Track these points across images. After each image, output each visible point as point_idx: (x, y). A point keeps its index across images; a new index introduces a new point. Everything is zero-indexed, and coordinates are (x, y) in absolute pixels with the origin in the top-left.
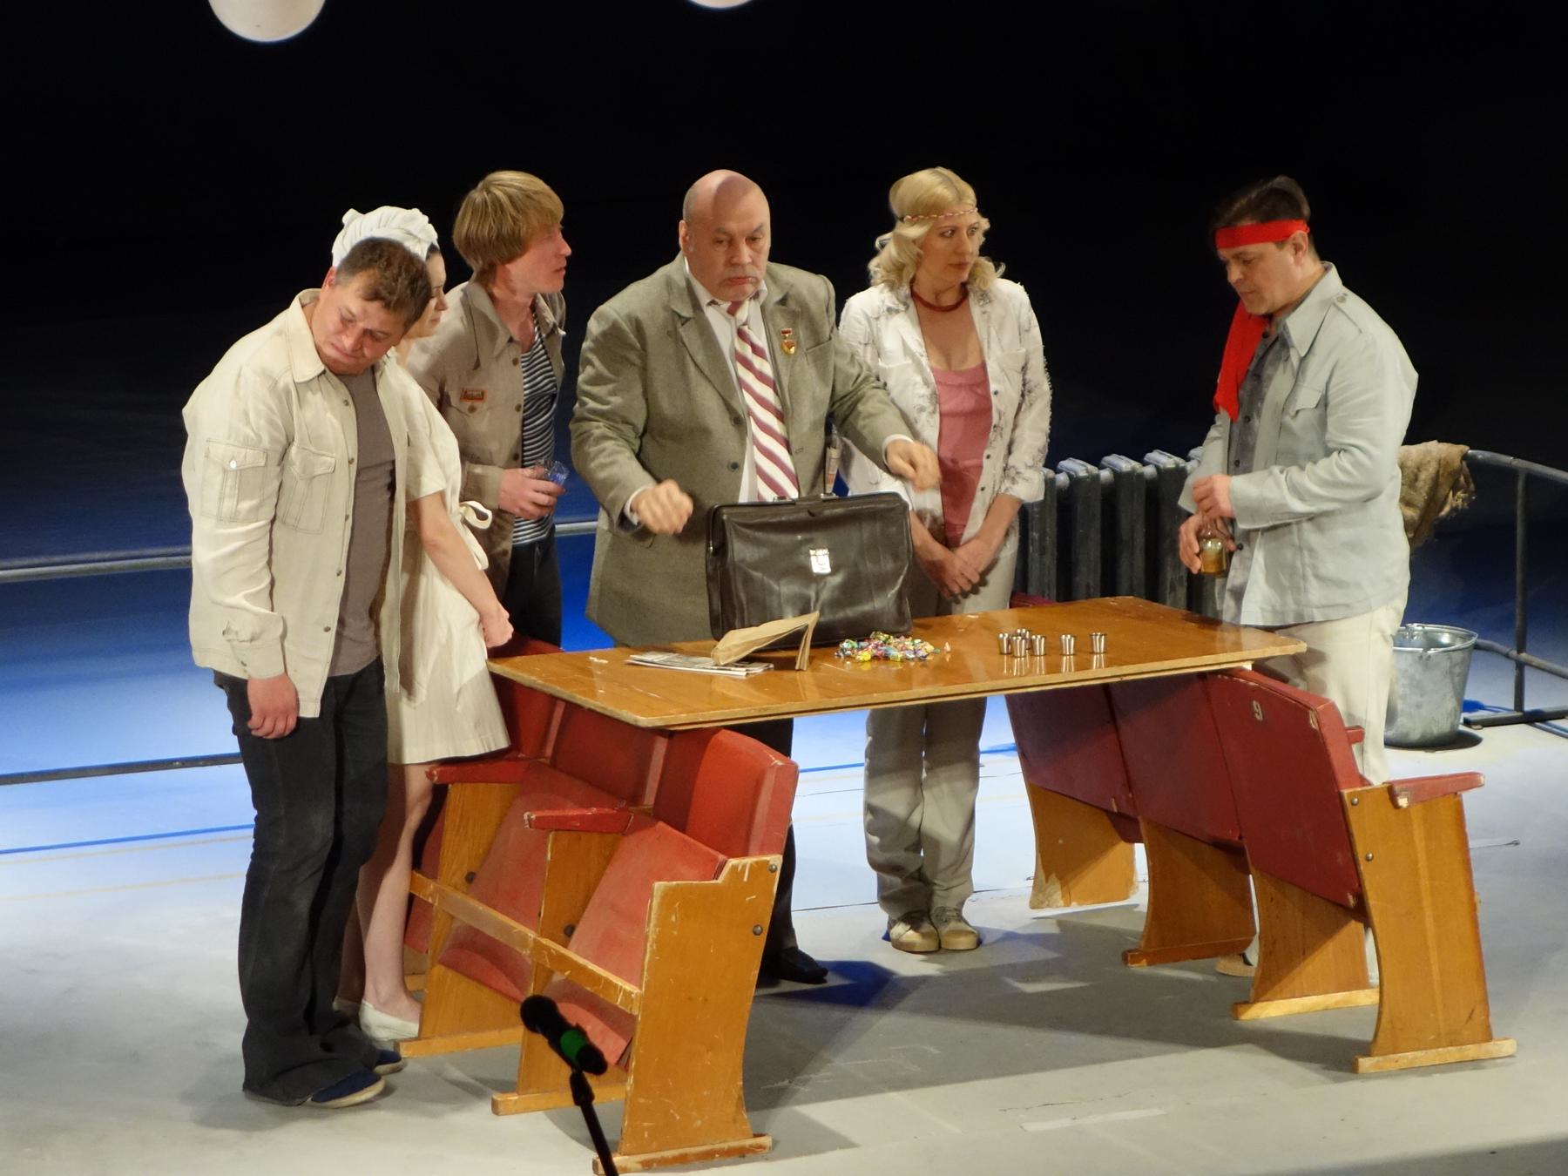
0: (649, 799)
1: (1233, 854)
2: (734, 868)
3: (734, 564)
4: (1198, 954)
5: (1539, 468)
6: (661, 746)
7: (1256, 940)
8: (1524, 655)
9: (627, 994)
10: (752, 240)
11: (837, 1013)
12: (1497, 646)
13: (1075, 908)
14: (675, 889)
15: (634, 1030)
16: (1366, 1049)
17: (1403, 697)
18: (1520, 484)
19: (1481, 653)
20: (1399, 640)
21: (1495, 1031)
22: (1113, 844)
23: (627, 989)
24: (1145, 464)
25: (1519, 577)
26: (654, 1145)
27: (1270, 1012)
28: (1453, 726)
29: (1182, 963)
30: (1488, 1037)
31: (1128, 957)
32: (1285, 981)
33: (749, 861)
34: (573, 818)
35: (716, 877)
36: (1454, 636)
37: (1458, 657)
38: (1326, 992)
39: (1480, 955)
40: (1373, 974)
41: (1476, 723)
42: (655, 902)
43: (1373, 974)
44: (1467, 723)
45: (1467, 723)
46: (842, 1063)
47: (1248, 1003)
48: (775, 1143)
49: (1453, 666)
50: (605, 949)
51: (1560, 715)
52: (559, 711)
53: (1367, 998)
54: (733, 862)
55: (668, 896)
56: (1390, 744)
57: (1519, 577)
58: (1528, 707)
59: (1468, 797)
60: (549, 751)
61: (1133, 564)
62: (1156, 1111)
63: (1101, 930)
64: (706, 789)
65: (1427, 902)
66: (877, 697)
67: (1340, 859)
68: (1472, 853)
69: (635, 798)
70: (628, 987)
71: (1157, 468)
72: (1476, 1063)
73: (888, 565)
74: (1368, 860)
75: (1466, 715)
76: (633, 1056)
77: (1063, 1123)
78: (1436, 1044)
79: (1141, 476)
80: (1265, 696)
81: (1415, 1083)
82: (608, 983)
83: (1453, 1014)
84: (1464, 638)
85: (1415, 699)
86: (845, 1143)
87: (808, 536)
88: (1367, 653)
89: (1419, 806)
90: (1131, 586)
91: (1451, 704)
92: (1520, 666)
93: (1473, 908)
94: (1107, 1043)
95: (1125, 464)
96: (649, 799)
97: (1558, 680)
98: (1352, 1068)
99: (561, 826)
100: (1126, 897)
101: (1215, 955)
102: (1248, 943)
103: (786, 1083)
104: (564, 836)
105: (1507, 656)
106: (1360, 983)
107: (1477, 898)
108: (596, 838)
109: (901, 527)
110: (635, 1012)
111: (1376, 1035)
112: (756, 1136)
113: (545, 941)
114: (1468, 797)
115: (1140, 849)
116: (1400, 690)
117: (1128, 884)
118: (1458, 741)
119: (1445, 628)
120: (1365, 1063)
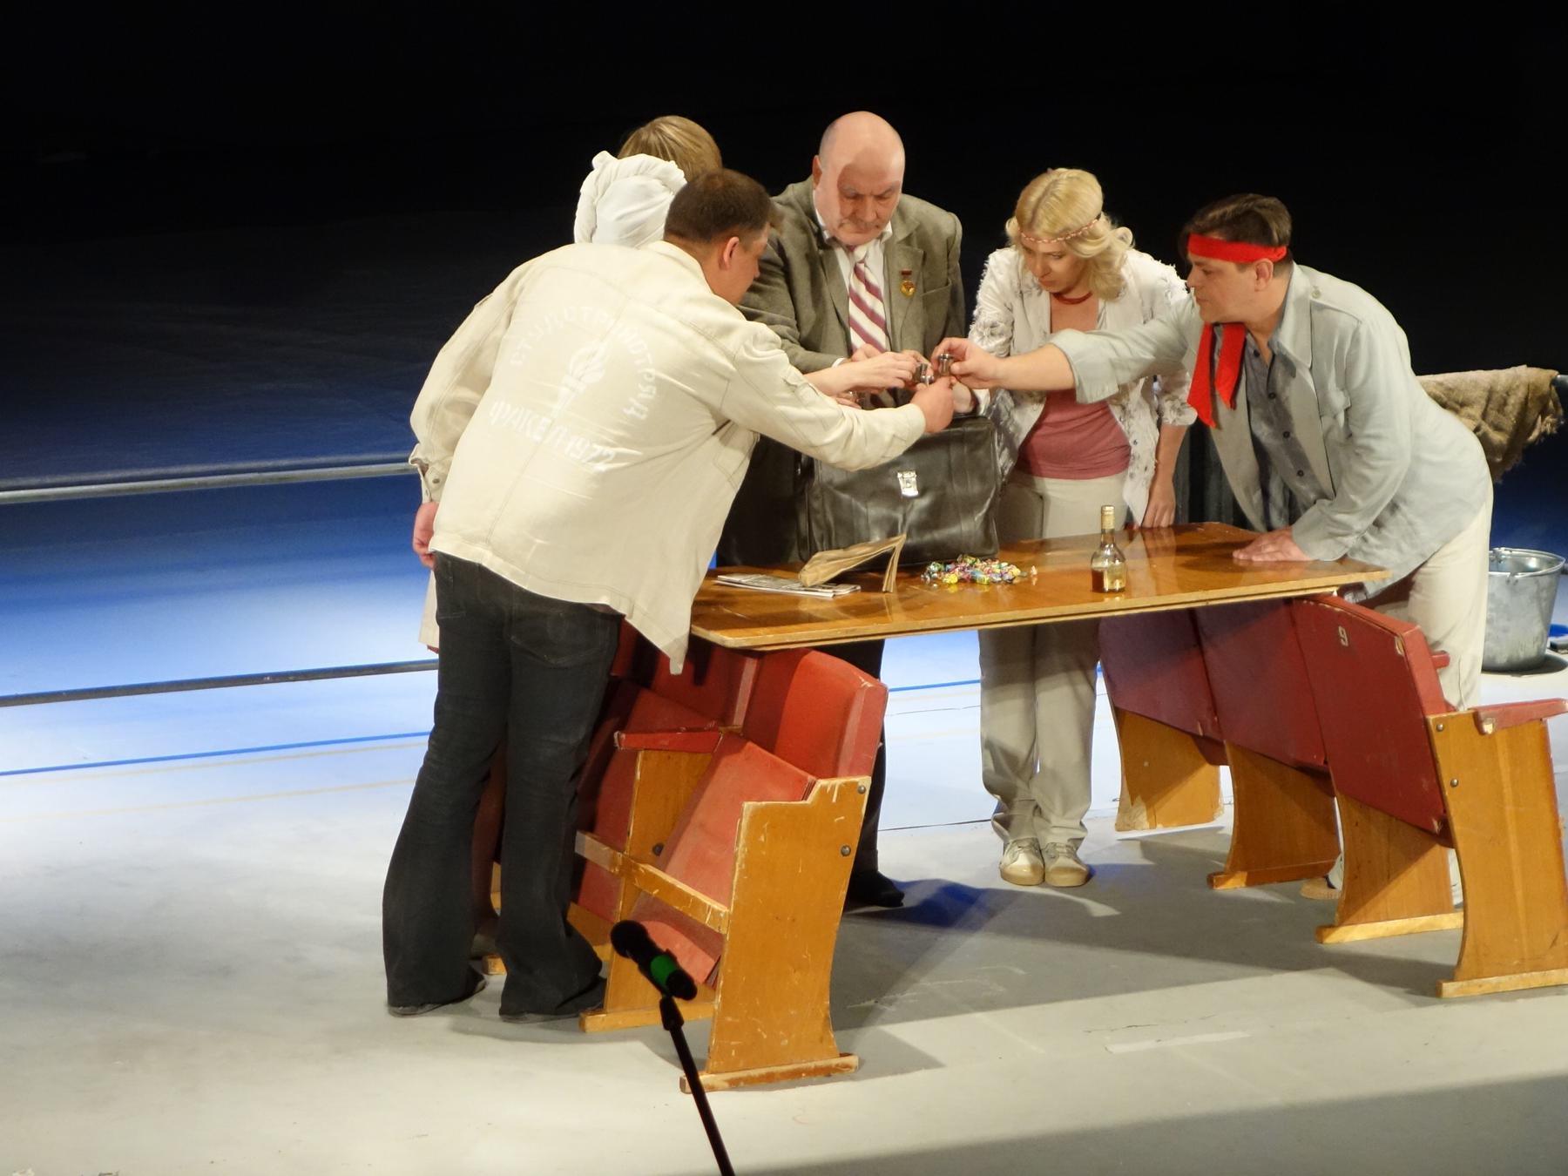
0: (738, 720)
1: (1319, 777)
2: (823, 789)
9: (716, 913)
11: (923, 934)
13: (1160, 830)
14: (763, 810)
15: (721, 949)
16: (1450, 974)
20: (1495, 563)
22: (1195, 768)
23: (715, 909)
26: (741, 1065)
27: (1353, 936)
32: (1368, 906)
35: (805, 797)
36: (1542, 561)
37: (1545, 581)
38: (1410, 916)
42: (745, 822)
44: (1554, 647)
45: (1554, 647)
46: (927, 984)
47: (1332, 927)
48: (861, 1062)
49: (1540, 590)
54: (822, 783)
55: (757, 816)
59: (1553, 723)
62: (1240, 1034)
66: (982, 618)
67: (1425, 784)
68: (1557, 778)
69: (725, 717)
73: (975, 488)
74: (1453, 785)
76: (721, 975)
77: (1148, 1045)
78: (1520, 969)
80: (1347, 619)
81: (1499, 1007)
82: (697, 902)
86: (929, 1063)
89: (1505, 733)
91: (1538, 628)
93: (1558, 833)
96: (738, 720)
98: (1436, 993)
100: (1211, 819)
102: (1330, 866)
104: (654, 755)
106: (1443, 907)
107: (1561, 824)
108: (684, 759)
110: (724, 931)
112: (842, 1055)
114: (1553, 723)
115: (1225, 772)
119: (1533, 553)
120: (1449, 988)
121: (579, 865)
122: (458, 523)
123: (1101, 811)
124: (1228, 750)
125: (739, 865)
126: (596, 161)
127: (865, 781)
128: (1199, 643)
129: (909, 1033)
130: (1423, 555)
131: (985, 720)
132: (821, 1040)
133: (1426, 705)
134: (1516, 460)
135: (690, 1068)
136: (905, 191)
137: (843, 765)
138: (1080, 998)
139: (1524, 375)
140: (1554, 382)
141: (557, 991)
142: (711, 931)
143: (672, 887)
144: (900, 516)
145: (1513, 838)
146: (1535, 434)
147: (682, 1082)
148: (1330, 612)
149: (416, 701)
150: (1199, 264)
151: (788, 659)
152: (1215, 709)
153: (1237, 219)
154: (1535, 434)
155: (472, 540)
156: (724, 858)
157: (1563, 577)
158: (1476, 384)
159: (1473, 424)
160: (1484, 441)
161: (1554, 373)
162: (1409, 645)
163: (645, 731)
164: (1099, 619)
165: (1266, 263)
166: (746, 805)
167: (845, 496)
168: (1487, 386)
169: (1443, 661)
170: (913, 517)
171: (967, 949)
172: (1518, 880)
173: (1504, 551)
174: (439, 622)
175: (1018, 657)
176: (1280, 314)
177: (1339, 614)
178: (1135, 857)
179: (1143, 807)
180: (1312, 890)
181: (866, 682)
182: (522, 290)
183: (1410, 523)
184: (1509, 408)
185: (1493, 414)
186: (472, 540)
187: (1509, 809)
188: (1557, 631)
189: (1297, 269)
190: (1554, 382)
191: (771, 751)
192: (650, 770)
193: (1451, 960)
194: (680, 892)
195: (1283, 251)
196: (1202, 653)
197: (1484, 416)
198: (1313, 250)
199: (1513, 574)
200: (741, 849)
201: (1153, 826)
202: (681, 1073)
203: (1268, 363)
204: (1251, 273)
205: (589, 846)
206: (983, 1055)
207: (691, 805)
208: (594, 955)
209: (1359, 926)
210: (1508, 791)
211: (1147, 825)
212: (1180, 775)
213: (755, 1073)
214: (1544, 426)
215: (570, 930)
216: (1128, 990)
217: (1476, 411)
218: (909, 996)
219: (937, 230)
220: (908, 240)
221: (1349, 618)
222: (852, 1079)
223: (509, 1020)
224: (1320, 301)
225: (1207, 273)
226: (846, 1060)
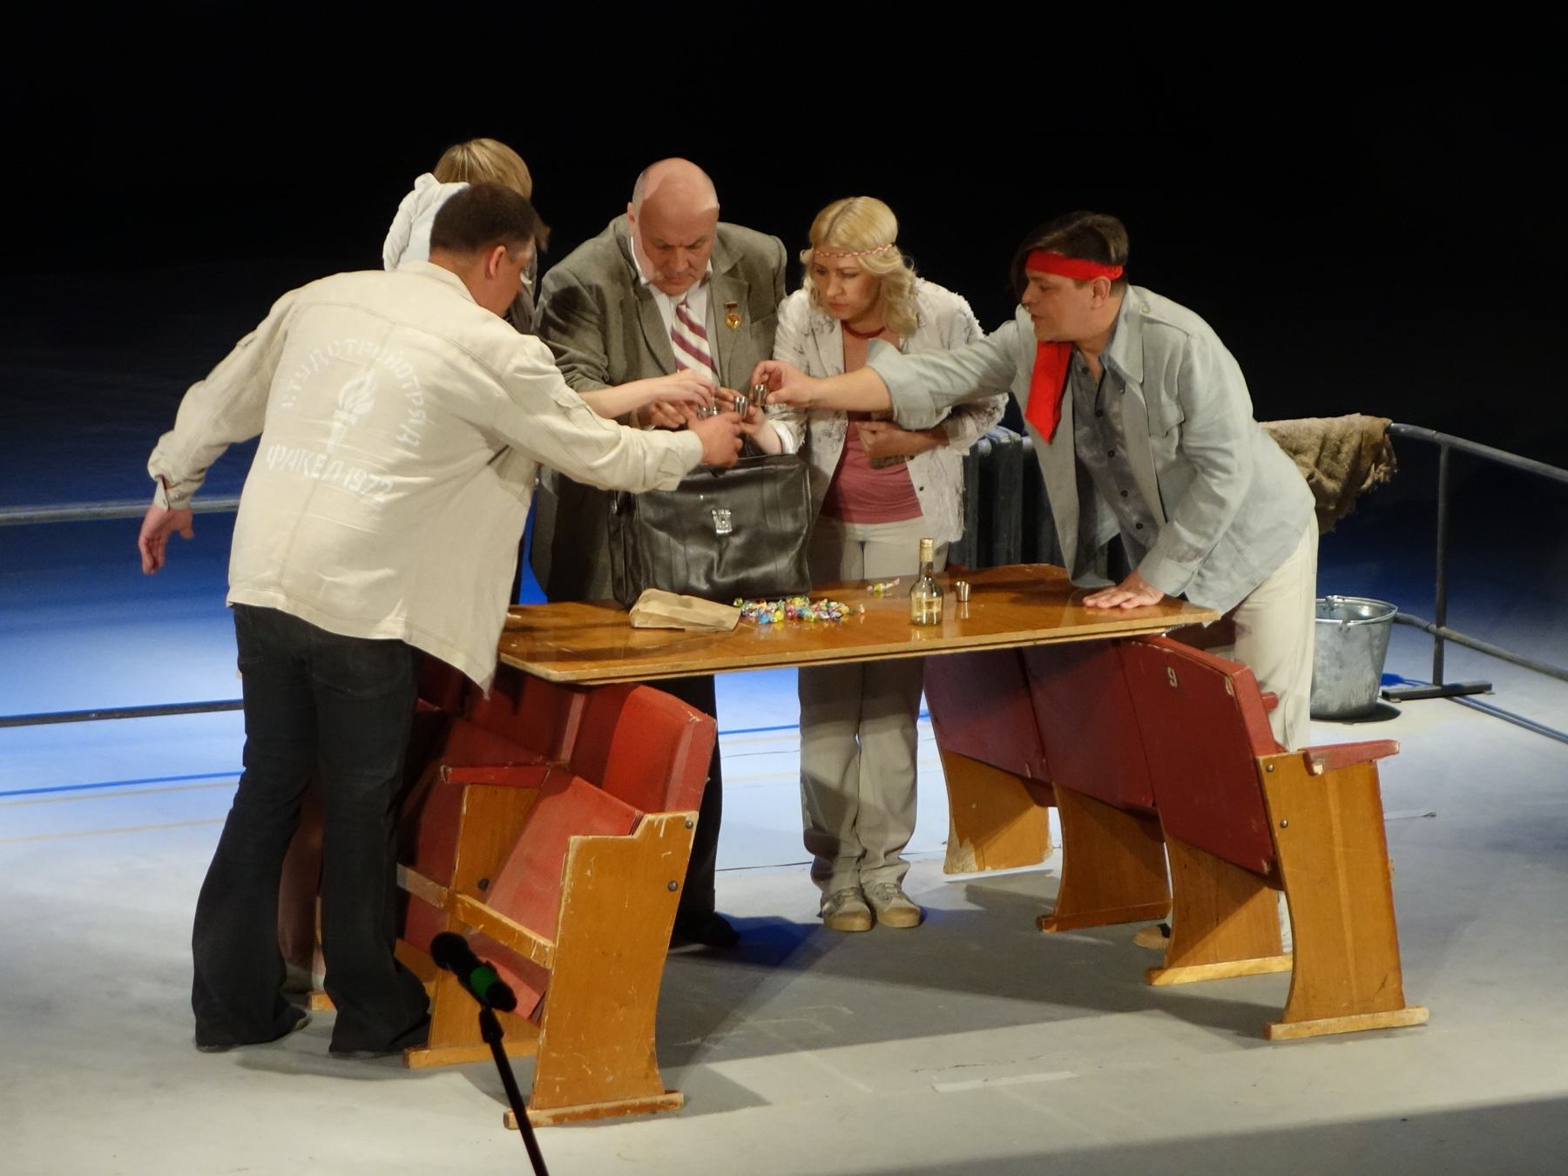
0: (566, 755)
1: (1147, 820)
2: (651, 823)
8: (1443, 629)
9: (541, 948)
12: (1417, 619)
13: (989, 872)
14: (589, 843)
15: (547, 983)
16: (1279, 1016)
20: (1325, 611)
22: (1026, 808)
23: (541, 943)
25: (1439, 551)
27: (1182, 978)
29: (1096, 929)
31: (1042, 922)
33: (665, 816)
35: (632, 832)
37: (1378, 629)
41: (1395, 696)
42: (571, 856)
43: (1288, 949)
44: (1386, 696)
45: (1386, 696)
47: (1161, 969)
48: (687, 1100)
49: (1372, 638)
50: (521, 904)
53: (1280, 965)
54: (649, 817)
55: (584, 849)
58: (1447, 681)
59: (1381, 764)
62: (1067, 1074)
68: (1387, 825)
69: (552, 752)
70: (542, 941)
72: (1387, 1031)
74: (1282, 826)
75: (1385, 688)
77: (973, 1084)
78: (1350, 1011)
81: (1326, 1050)
82: (522, 938)
85: (1335, 671)
86: (755, 1100)
91: (1370, 676)
92: (1440, 640)
93: (1387, 875)
96: (566, 755)
98: (1265, 1035)
100: (1040, 860)
103: (698, 1040)
105: (1427, 630)
106: (1273, 949)
107: (1390, 866)
108: (512, 792)
110: (549, 966)
112: (668, 1092)
114: (1381, 764)
115: (1053, 813)
117: (1039, 850)
119: (1366, 601)
120: (1278, 1030)
121: (403, 899)
122: (269, 562)
123: (927, 852)
125: (565, 900)
127: (693, 816)
128: (1027, 684)
129: (735, 1071)
130: (1253, 583)
131: (805, 756)
133: (1256, 745)
134: (1349, 508)
135: (517, 1102)
136: (720, 220)
137: (669, 803)
139: (1356, 423)
140: (1388, 430)
141: (384, 1030)
143: (498, 921)
144: (714, 554)
146: (1369, 482)
147: (506, 1118)
148: (1160, 652)
149: (224, 741)
150: (1036, 279)
151: (615, 694)
152: (1043, 751)
153: (1071, 239)
154: (1369, 482)
155: (265, 585)
156: (556, 890)
157: (1395, 626)
158: (1309, 431)
159: (1307, 472)
160: (1316, 488)
161: (1387, 421)
162: (1239, 688)
163: (473, 766)
164: (922, 659)
165: (1104, 281)
166: (573, 839)
167: (662, 535)
168: (1321, 433)
169: (1272, 703)
170: (729, 555)
171: (795, 991)
172: (1347, 923)
173: (1337, 599)
174: (242, 667)
175: (842, 696)
176: (1112, 331)
177: (1169, 655)
178: (960, 903)
179: (971, 847)
181: (695, 717)
182: (286, 335)
183: (1239, 551)
184: (1342, 456)
185: (1326, 461)
186: (265, 585)
187: (1339, 850)
189: (1130, 289)
190: (1388, 430)
191: (599, 786)
192: (474, 804)
194: (506, 927)
195: (1120, 271)
196: (1031, 696)
197: (1318, 463)
198: (1141, 273)
199: (1345, 622)
200: (567, 883)
201: (982, 869)
202: (504, 1109)
203: (1097, 380)
204: (1088, 291)
205: (410, 879)
207: (515, 840)
208: (423, 989)
210: (1338, 837)
211: (975, 866)
212: (1006, 817)
214: (1377, 474)
215: (398, 964)
216: (956, 1030)
217: (1310, 459)
218: (735, 1034)
219: (762, 259)
220: (732, 272)
222: (678, 1116)
223: (339, 1057)
224: (1150, 316)
225: (1043, 289)
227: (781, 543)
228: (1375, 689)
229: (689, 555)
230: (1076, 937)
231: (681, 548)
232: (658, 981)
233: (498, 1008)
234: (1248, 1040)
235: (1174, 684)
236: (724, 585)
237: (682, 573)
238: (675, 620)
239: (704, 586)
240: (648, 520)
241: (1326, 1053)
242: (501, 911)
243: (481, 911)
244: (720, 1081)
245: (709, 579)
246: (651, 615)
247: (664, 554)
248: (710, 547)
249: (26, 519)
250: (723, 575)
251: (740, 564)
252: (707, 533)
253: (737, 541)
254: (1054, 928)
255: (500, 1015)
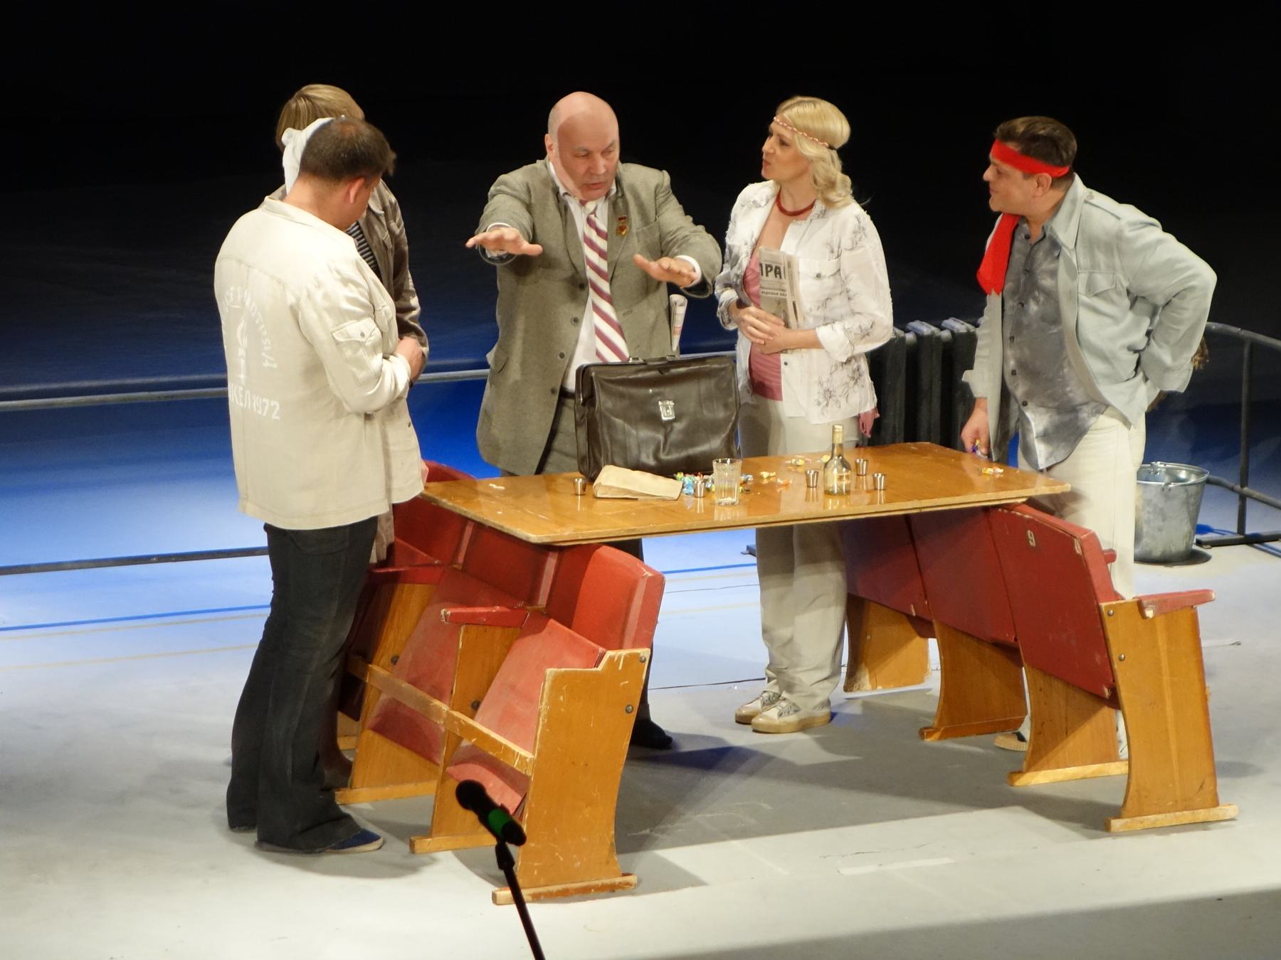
0: (542, 601)
1: (1010, 652)
2: (611, 658)
3: (601, 413)
4: (981, 731)
5: (1261, 338)
6: (551, 562)
7: (1027, 719)
8: (1246, 489)
9: (523, 759)
10: (606, 152)
11: (689, 775)
12: (1225, 481)
13: (880, 690)
14: (563, 675)
15: (528, 787)
16: (1117, 812)
17: (1148, 522)
18: (1246, 351)
19: (1215, 488)
20: (1143, 475)
21: (1221, 799)
22: (909, 639)
23: (522, 754)
24: (942, 329)
25: (1243, 425)
26: (542, 881)
27: (1039, 780)
28: (1188, 545)
29: (967, 738)
30: (1216, 804)
31: (924, 732)
32: (1050, 755)
33: (623, 653)
34: (481, 614)
35: (597, 665)
36: (1190, 473)
37: (1193, 490)
38: (1084, 764)
39: (1210, 735)
40: (1124, 752)
41: (1207, 543)
42: (547, 685)
43: (1124, 752)
44: (1199, 543)
45: (1199, 543)
46: (697, 818)
47: (1021, 772)
48: (640, 881)
49: (1188, 497)
50: (506, 721)
51: (1275, 538)
52: (469, 530)
53: (1117, 769)
54: (610, 653)
55: (558, 679)
56: (1142, 559)
57: (1243, 425)
58: (1248, 531)
59: (1201, 609)
60: (461, 559)
61: (930, 412)
62: (946, 860)
63: (901, 710)
64: (574, 591)
65: (1168, 693)
66: (760, 518)
67: (1098, 658)
68: (1204, 651)
69: (531, 598)
70: (524, 753)
71: (952, 333)
72: (1204, 825)
73: (721, 414)
74: (1121, 660)
75: (1198, 537)
76: (527, 810)
77: (871, 868)
78: (1175, 808)
79: (939, 338)
80: (1033, 525)
81: (1155, 840)
82: (507, 749)
83: (1192, 784)
84: (1198, 475)
85: (1159, 523)
86: (695, 882)
87: (657, 390)
88: (1110, 483)
89: (1163, 617)
90: (929, 432)
91: (1186, 527)
92: (1243, 498)
93: (1205, 699)
94: (906, 804)
95: (926, 329)
96: (542, 601)
97: (1274, 510)
98: (1106, 828)
99: (471, 621)
100: (922, 681)
101: (993, 731)
102: (1021, 722)
103: (648, 831)
104: (473, 628)
105: (1232, 489)
106: (1111, 757)
107: (1208, 691)
108: (499, 631)
109: (729, 383)
110: (529, 773)
111: (1125, 802)
112: (624, 875)
113: (456, 714)
114: (1201, 609)
115: (933, 644)
116: (1145, 516)
117: (920, 672)
118: (1192, 557)
119: (1183, 466)
120: (1116, 824)
124: (936, 627)
126: (284, 138)
132: (607, 863)
138: (815, 829)
142: (520, 774)
144: (661, 437)
145: (1169, 703)
148: (1021, 518)
157: (1208, 487)
162: (1086, 546)
167: (619, 421)
169: (1111, 557)
171: (729, 792)
177: (1029, 521)
180: (1005, 741)
188: (1203, 529)
193: (1119, 801)
201: (874, 688)
206: (732, 875)
209: (1042, 773)
213: (554, 888)
221: (1037, 524)
222: (633, 894)
226: (627, 879)
227: (713, 428)
228: (1191, 538)
229: (640, 437)
230: (950, 744)
231: (634, 432)
232: (616, 787)
233: (511, 842)
234: (1094, 832)
235: (1033, 543)
236: (668, 462)
237: (635, 452)
238: (629, 492)
239: (652, 462)
240: (607, 409)
241: (1154, 842)
242: (489, 728)
243: (473, 728)
244: (666, 864)
245: (656, 457)
246: (610, 488)
247: (620, 437)
248: (658, 432)
249: (100, 401)
250: (668, 454)
251: (680, 445)
252: (653, 419)
253: (678, 426)
254: (937, 735)
255: (512, 848)
